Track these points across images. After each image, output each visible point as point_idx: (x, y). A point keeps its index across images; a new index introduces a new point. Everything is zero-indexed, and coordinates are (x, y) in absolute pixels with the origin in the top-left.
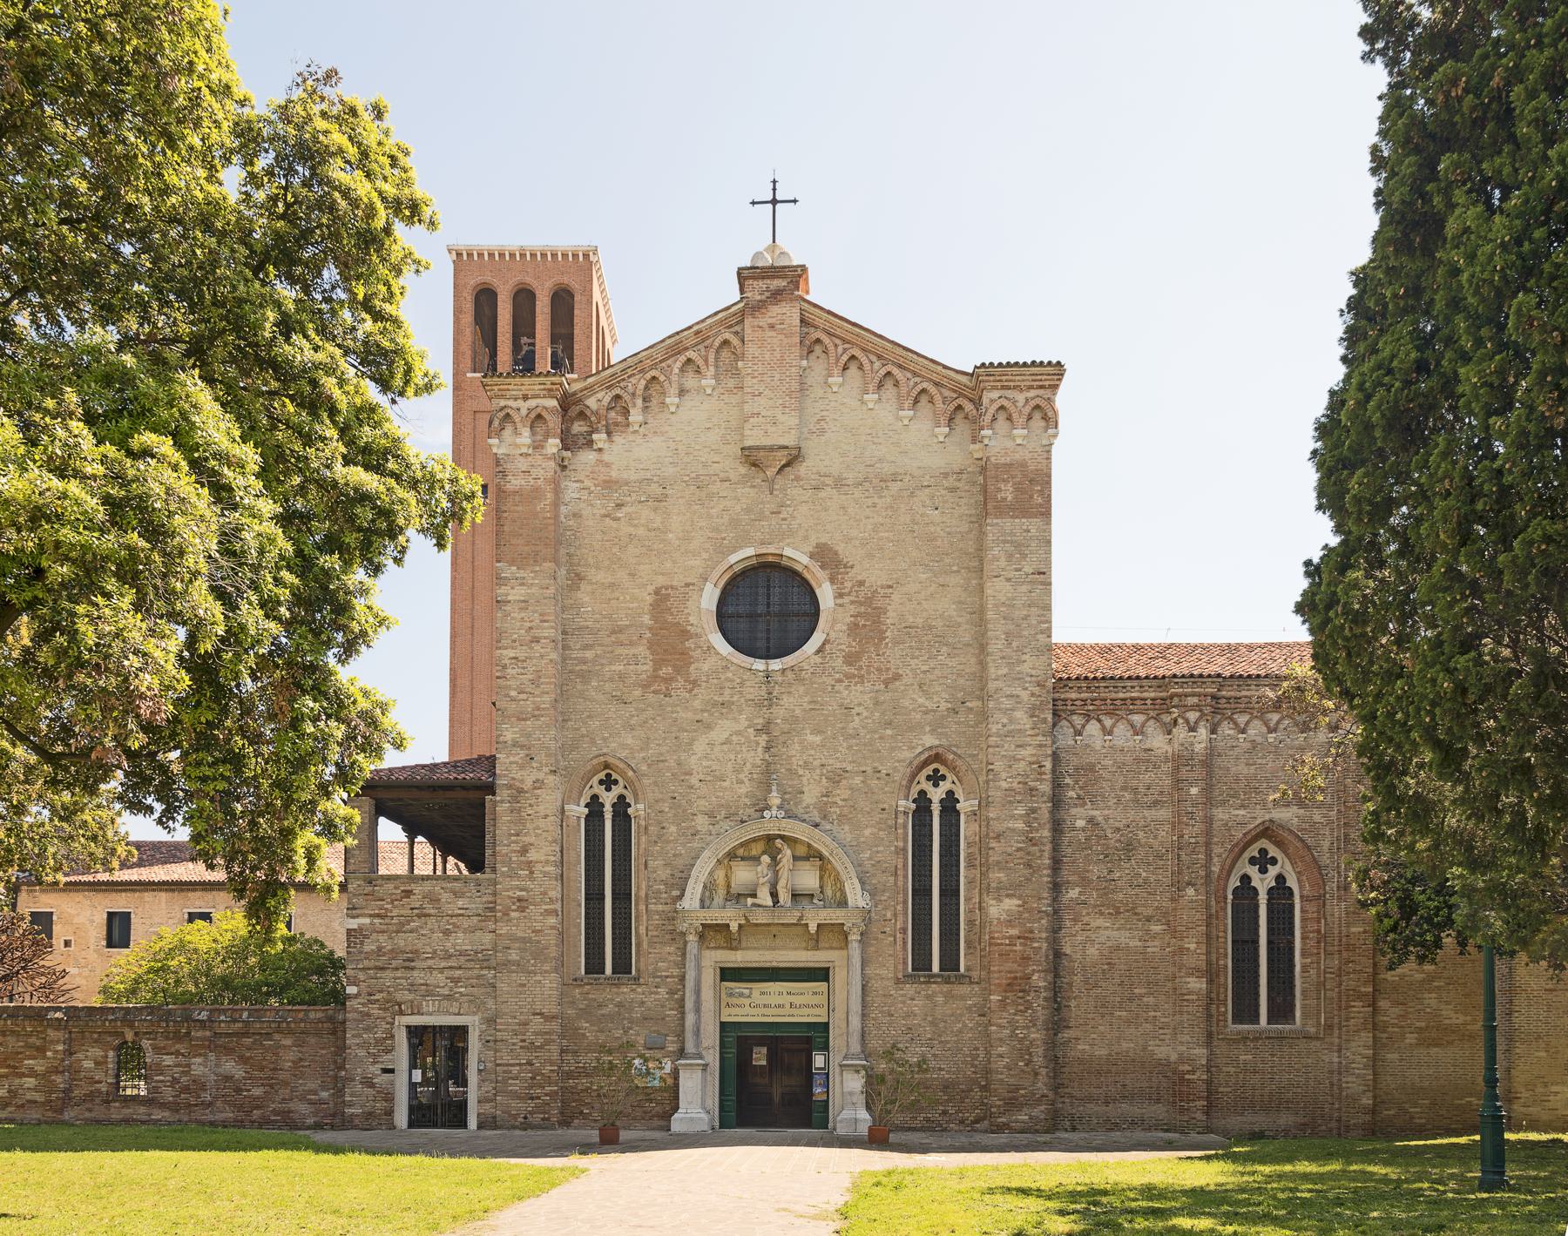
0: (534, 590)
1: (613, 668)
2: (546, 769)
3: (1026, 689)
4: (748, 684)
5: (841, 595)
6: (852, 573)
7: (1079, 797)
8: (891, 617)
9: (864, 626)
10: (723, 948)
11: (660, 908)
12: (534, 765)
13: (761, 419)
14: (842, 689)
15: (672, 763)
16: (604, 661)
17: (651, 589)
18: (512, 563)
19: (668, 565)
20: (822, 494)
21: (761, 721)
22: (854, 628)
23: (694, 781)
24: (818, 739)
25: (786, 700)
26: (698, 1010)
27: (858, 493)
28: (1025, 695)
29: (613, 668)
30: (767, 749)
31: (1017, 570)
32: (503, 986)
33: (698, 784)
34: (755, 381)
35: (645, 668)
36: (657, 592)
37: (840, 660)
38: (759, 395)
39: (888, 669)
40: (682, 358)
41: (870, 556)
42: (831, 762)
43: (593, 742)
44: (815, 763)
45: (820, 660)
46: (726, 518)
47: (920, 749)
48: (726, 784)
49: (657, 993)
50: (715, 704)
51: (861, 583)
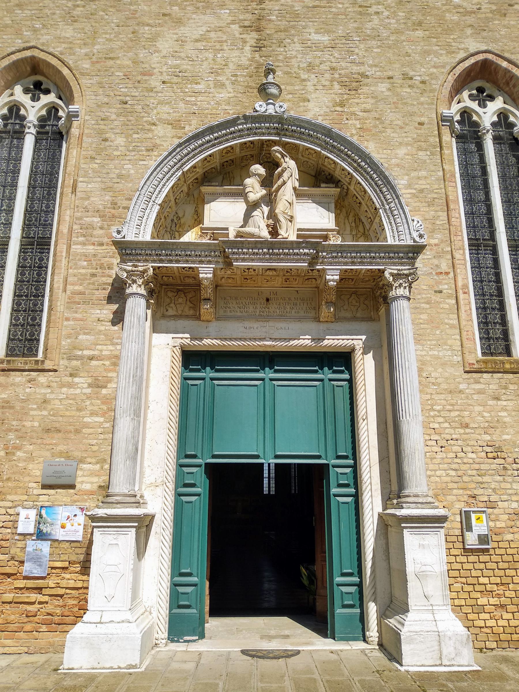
10: (187, 317)
11: (90, 249)
23: (155, 82)
24: (325, 39)
30: (258, 48)
33: (160, 86)
42: (343, 64)
43: (18, 33)
44: (322, 67)
47: (462, 55)
48: (201, 87)
49: (70, 386)
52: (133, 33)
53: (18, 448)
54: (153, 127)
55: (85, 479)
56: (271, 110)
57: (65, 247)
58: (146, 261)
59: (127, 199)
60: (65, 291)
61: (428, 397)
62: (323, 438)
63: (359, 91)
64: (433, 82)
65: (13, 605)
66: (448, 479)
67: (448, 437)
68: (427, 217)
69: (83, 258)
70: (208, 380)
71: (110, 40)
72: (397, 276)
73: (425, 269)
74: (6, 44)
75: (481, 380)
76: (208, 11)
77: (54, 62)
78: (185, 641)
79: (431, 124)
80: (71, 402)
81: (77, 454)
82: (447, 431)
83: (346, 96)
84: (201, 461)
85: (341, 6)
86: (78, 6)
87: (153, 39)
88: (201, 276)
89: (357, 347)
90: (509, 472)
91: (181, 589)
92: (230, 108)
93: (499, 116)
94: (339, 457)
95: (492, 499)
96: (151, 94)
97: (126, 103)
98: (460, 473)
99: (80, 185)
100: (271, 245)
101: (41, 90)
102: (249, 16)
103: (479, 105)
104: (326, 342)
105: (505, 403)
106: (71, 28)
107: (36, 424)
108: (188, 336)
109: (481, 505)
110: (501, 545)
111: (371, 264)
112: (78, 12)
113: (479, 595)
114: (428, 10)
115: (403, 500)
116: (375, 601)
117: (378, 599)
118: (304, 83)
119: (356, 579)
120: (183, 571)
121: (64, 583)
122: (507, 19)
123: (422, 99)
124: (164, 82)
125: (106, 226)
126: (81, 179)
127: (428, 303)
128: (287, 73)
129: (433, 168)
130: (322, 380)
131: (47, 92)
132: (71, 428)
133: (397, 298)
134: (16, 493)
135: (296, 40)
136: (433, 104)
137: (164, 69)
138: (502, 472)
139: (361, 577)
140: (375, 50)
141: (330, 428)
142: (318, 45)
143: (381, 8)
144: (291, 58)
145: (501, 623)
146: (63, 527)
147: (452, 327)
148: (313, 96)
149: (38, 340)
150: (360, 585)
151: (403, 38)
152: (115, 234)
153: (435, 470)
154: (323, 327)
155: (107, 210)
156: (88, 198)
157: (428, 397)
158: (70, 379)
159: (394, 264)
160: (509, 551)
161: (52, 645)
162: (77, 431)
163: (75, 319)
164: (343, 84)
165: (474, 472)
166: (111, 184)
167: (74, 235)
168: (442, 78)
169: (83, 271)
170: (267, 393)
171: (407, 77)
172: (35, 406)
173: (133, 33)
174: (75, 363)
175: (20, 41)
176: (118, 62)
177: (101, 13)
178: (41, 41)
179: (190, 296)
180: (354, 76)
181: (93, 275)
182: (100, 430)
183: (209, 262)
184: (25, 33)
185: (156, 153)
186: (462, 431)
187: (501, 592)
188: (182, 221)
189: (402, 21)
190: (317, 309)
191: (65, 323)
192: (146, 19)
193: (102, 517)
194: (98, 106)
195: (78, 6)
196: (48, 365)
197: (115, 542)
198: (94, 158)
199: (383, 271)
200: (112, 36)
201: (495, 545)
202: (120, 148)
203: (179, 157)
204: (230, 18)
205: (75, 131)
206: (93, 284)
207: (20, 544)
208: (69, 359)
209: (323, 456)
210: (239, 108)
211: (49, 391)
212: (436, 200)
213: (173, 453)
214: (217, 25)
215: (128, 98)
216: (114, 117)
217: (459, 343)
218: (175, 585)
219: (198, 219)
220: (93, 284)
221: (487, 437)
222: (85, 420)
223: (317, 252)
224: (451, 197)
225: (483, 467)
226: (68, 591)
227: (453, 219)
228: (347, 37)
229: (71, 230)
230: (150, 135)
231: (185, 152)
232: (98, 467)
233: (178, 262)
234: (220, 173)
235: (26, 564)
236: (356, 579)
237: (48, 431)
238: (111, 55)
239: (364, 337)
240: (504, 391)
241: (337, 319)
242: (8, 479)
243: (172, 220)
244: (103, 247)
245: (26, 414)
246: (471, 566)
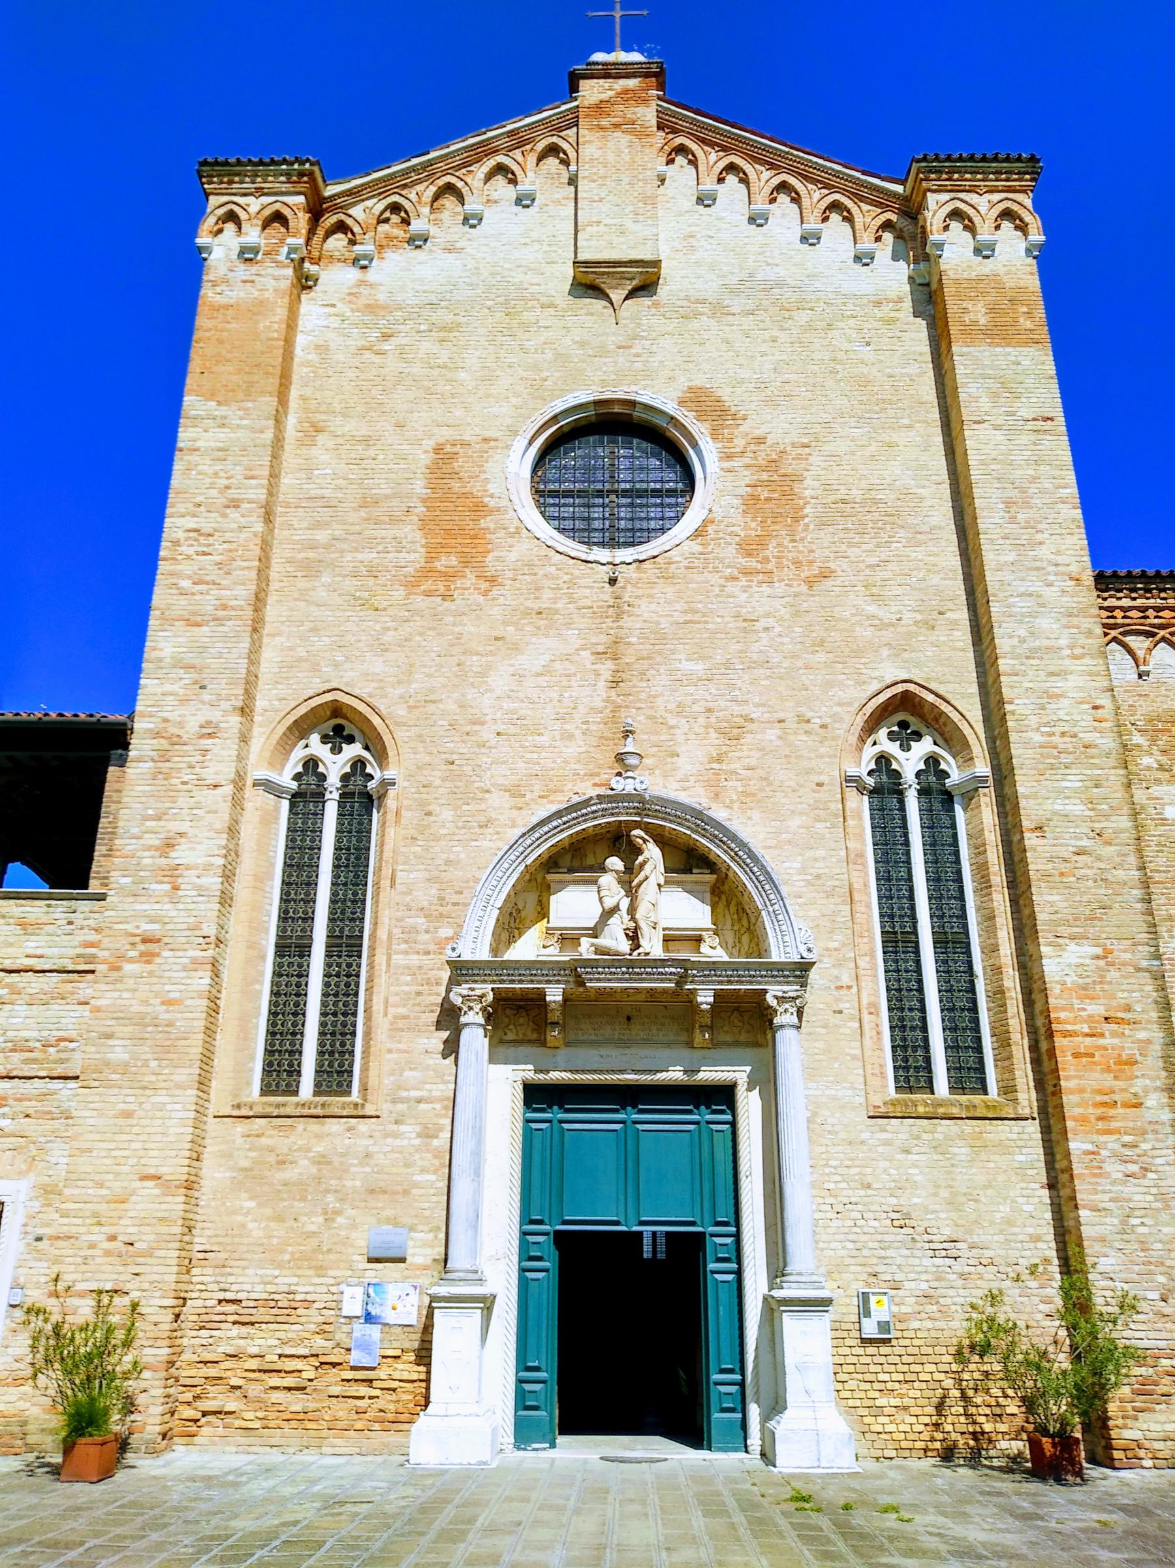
0: (240, 434)
1: (360, 557)
2: (226, 705)
3: (1051, 585)
4: (582, 582)
5: (729, 457)
6: (745, 427)
7: (1161, 768)
8: (809, 488)
9: (768, 499)
10: (530, 1042)
11: (414, 960)
12: (206, 696)
13: (601, 228)
14: (737, 592)
15: (453, 707)
16: (345, 546)
17: (429, 444)
18: (211, 396)
19: (459, 413)
20: (695, 325)
21: (603, 638)
22: (751, 503)
23: (487, 734)
24: (699, 667)
25: (645, 609)
26: (477, 1172)
27: (748, 322)
28: (1051, 593)
29: (360, 557)
30: (615, 683)
31: (1009, 414)
32: (1048, 1340)
33: (493, 740)
34: (593, 185)
35: (412, 556)
36: (438, 450)
37: (732, 550)
38: (601, 200)
39: (811, 562)
40: (491, 163)
41: (771, 402)
42: (723, 704)
43: (316, 668)
44: (695, 708)
45: (699, 548)
46: (549, 355)
47: (875, 686)
48: (544, 739)
49: (396, 1135)
50: (526, 613)
51: (760, 440)
52: (459, 665)
53: (338, 1212)
54: (487, 795)
55: (417, 1250)
56: (629, 789)
57: (385, 957)
58: (485, 981)
59: (456, 893)
60: (386, 1014)
61: (823, 1149)
62: (699, 1199)
63: (742, 741)
64: (837, 725)
65: (341, 1399)
66: (844, 1253)
67: (846, 1201)
68: (825, 912)
69: (407, 971)
70: (555, 1122)
71: (429, 676)
72: (781, 999)
73: (821, 982)
74: (301, 686)
75: (888, 1128)
76: (552, 632)
77: (361, 707)
78: (534, 1450)
79: (832, 785)
80: (397, 1155)
81: (407, 1221)
82: (845, 1193)
83: (724, 748)
84: (548, 1227)
85: (719, 620)
86: (388, 629)
87: (483, 674)
88: (548, 998)
89: (740, 1082)
90: (919, 1245)
91: (527, 1387)
92: (581, 767)
93: (926, 762)
94: (718, 1224)
95: (898, 1277)
96: (483, 750)
97: (453, 763)
98: (859, 1245)
99: (399, 874)
100: (631, 964)
101: (342, 737)
102: (603, 638)
104: (701, 1075)
105: (916, 1157)
106: (381, 659)
107: (358, 1183)
108: (531, 1067)
109: (883, 1284)
110: (906, 1334)
111: (751, 983)
112: (388, 637)
113: (877, 1394)
114: (833, 623)
115: (785, 1279)
116: (757, 1402)
117: (761, 1400)
118: (672, 731)
119: (738, 1377)
120: (530, 1364)
121: (397, 1375)
122: (937, 633)
123: (822, 750)
124: (498, 734)
125: (432, 929)
126: (401, 867)
127: (824, 1027)
128: (650, 718)
129: (833, 845)
130: (697, 1123)
131: (350, 740)
132: (399, 1188)
133: (782, 1026)
134: (338, 1268)
135: (662, 671)
136: (835, 756)
137: (499, 715)
138: (910, 1245)
139: (743, 1374)
140: (763, 682)
141: (707, 1186)
142: (689, 677)
143: (771, 622)
144: (655, 697)
145: (902, 1428)
146: (394, 1309)
147: (854, 1058)
148: (684, 748)
149: (350, 1072)
150: (742, 1384)
151: (799, 664)
152: (449, 952)
153: (829, 1242)
154: (698, 1054)
155: (433, 907)
156: (410, 893)
157: (823, 1149)
158: (394, 1127)
159: (779, 983)
160: (916, 1342)
161: (386, 1445)
162: (406, 1192)
163: (399, 1051)
164: (720, 731)
165: (876, 1245)
166: (436, 873)
167: (394, 942)
168: (848, 719)
169: (406, 988)
170: (629, 1142)
172: (356, 1162)
173: (459, 665)
174: (400, 1107)
175: (318, 680)
176: (441, 706)
177: (418, 638)
178: (344, 680)
179: (533, 1014)
180: (737, 720)
181: (419, 993)
182: (432, 1191)
183: (558, 982)
184: (324, 669)
185: (490, 830)
186: (862, 1192)
187: (904, 1391)
188: (523, 914)
189: (799, 640)
190: (690, 1030)
191: (388, 1056)
193: (444, 1297)
194: (418, 768)
195: (388, 629)
196: (369, 1110)
197: (458, 1325)
198: (416, 839)
199: (765, 991)
200: (433, 669)
201: (899, 1334)
202: (448, 825)
203: (521, 849)
204: (580, 642)
205: (391, 802)
206: (419, 1005)
207: (346, 1328)
208: (394, 1101)
209: (699, 1223)
210: (591, 767)
211: (372, 1142)
212: (837, 889)
213: (516, 1219)
214: (564, 652)
215: (455, 757)
216: (438, 782)
217: (862, 1080)
218: (520, 1381)
219: (543, 912)
220: (419, 1005)
221: (894, 1201)
222: (416, 1178)
223: (686, 970)
224: (855, 886)
225: (886, 1238)
226: (402, 1384)
227: (858, 915)
228: (727, 665)
229: (390, 934)
230: (484, 807)
231: (529, 842)
232: (431, 1235)
233: (521, 982)
234: (569, 850)
235: (353, 1352)
236: (738, 1377)
237: (372, 1191)
238: (432, 697)
239: (748, 1069)
240: (915, 1142)
241: (714, 1044)
242: (329, 1251)
243: (511, 914)
244: (430, 957)
245: (346, 1171)
246: (868, 1360)
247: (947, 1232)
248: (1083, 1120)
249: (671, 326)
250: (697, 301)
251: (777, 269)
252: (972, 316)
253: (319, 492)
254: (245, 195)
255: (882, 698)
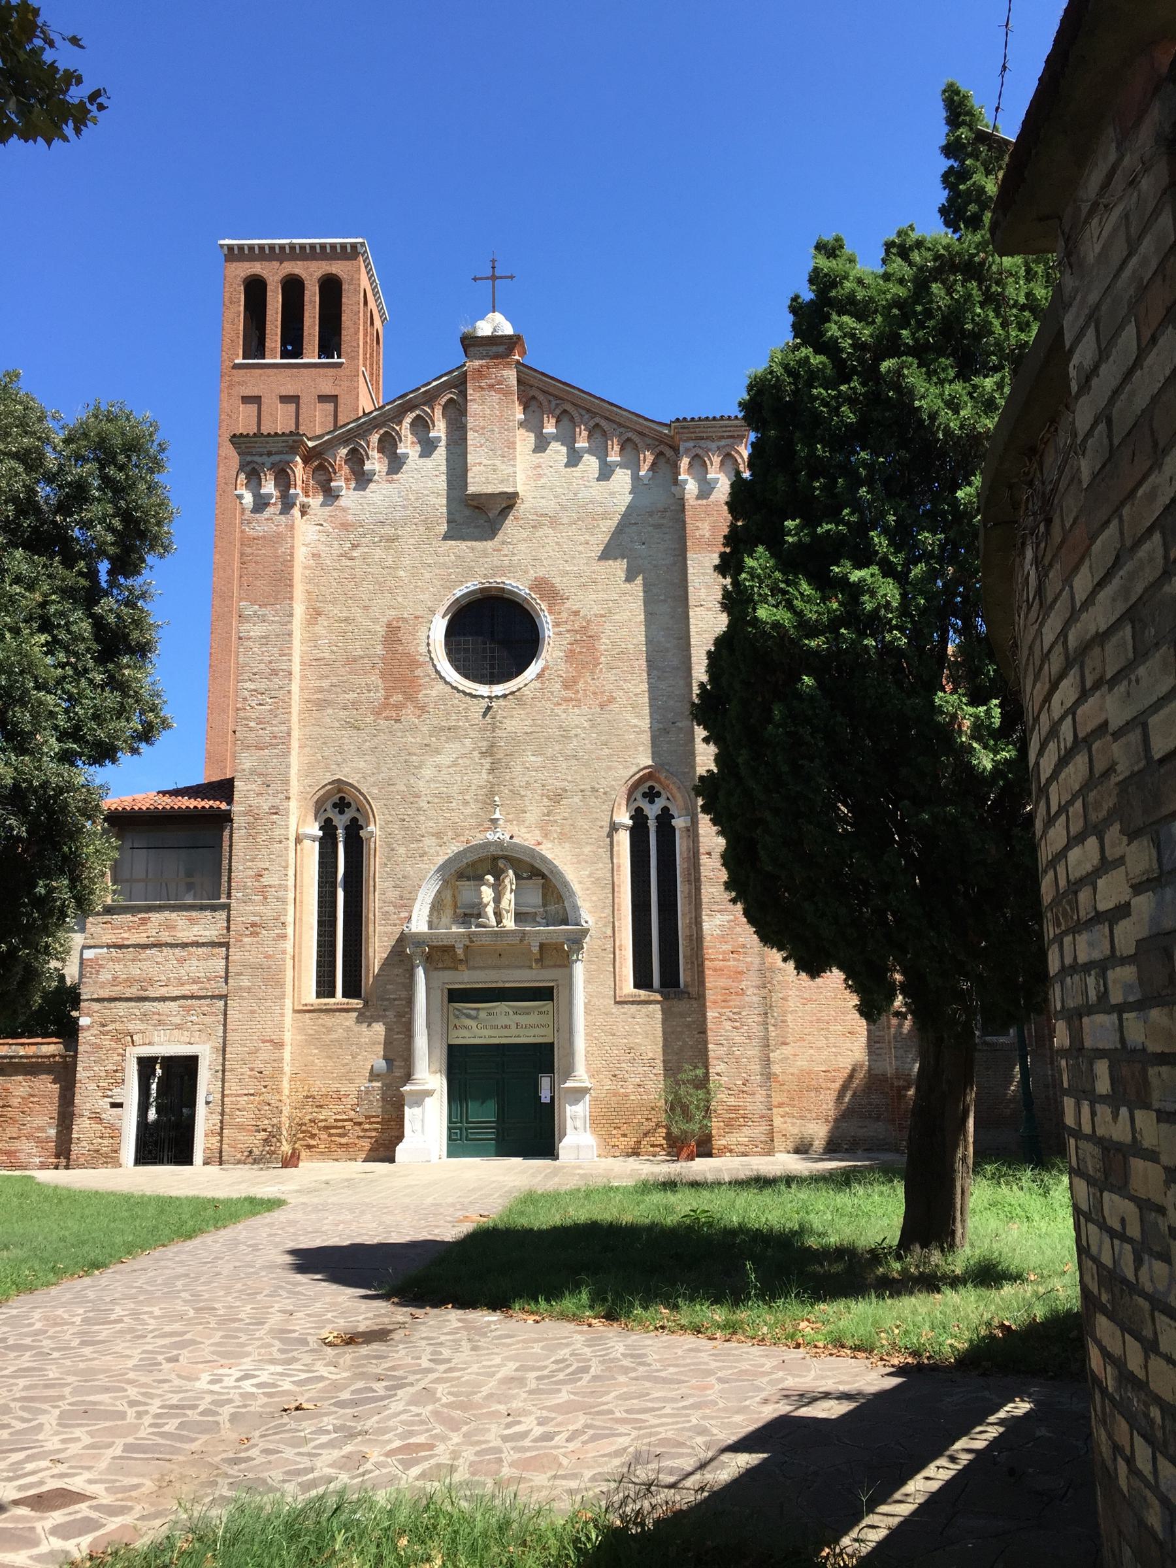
6: (568, 604)
8: (604, 643)
9: (580, 653)
21: (485, 743)
22: (570, 656)
30: (492, 770)
36: (389, 625)
37: (558, 686)
45: (539, 685)
47: (635, 769)
50: (442, 729)
51: (576, 613)
103: (642, 810)
128: (510, 791)
171: (594, 790)
192: (413, 750)
208: (383, 1000)
247: (651, 1055)
248: (715, 1002)
249: (525, 534)
250: (542, 515)
251: (591, 490)
252: (701, 532)
253: (322, 655)
254: (261, 455)
255: (637, 777)
